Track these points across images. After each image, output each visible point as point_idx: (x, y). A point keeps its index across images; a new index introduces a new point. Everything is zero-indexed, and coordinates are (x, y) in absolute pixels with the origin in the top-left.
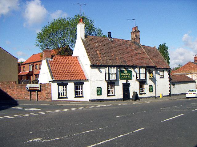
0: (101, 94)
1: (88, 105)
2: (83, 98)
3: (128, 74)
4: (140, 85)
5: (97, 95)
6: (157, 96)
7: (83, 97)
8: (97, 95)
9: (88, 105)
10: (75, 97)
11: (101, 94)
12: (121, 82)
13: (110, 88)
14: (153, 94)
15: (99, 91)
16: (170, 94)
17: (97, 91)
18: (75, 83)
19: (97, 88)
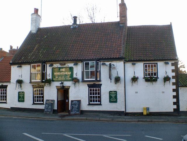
0: (23, 101)
1: (68, 118)
2: (101, 106)
3: (66, 73)
4: (69, 89)
5: (19, 101)
6: (127, 112)
7: (6, 103)
8: (19, 101)
9: (68, 118)
10: (34, 104)
11: (23, 101)
12: (57, 84)
13: (3, 93)
14: (118, 107)
15: (21, 97)
16: (177, 110)
17: (19, 97)
18: (89, 86)
19: (110, 92)
